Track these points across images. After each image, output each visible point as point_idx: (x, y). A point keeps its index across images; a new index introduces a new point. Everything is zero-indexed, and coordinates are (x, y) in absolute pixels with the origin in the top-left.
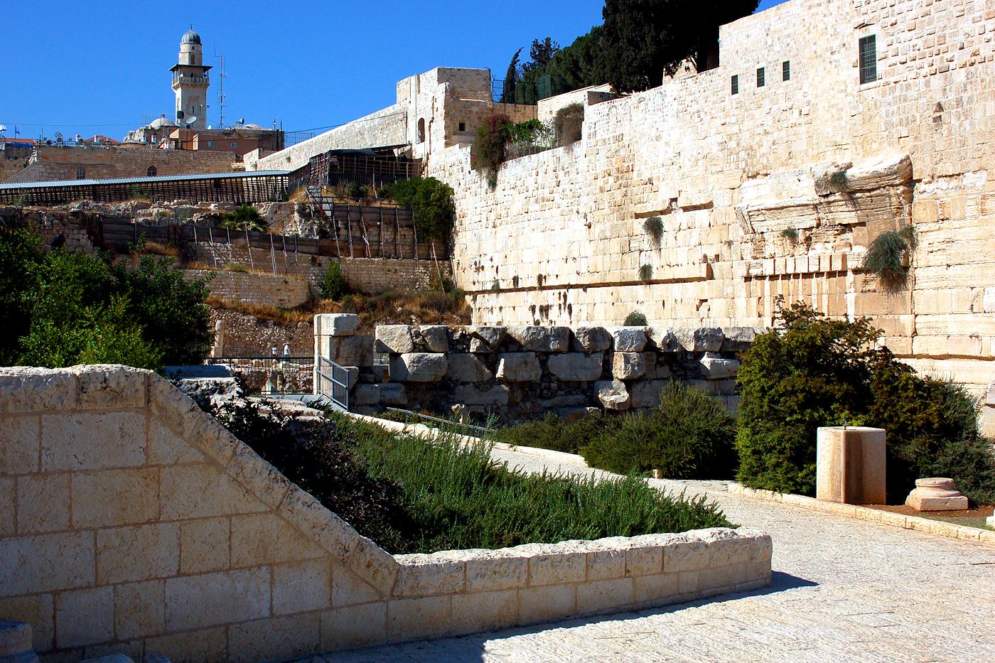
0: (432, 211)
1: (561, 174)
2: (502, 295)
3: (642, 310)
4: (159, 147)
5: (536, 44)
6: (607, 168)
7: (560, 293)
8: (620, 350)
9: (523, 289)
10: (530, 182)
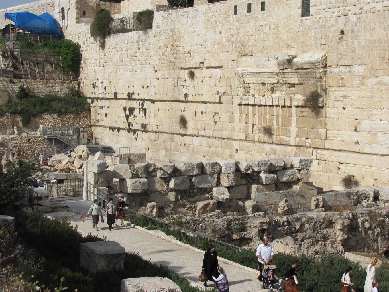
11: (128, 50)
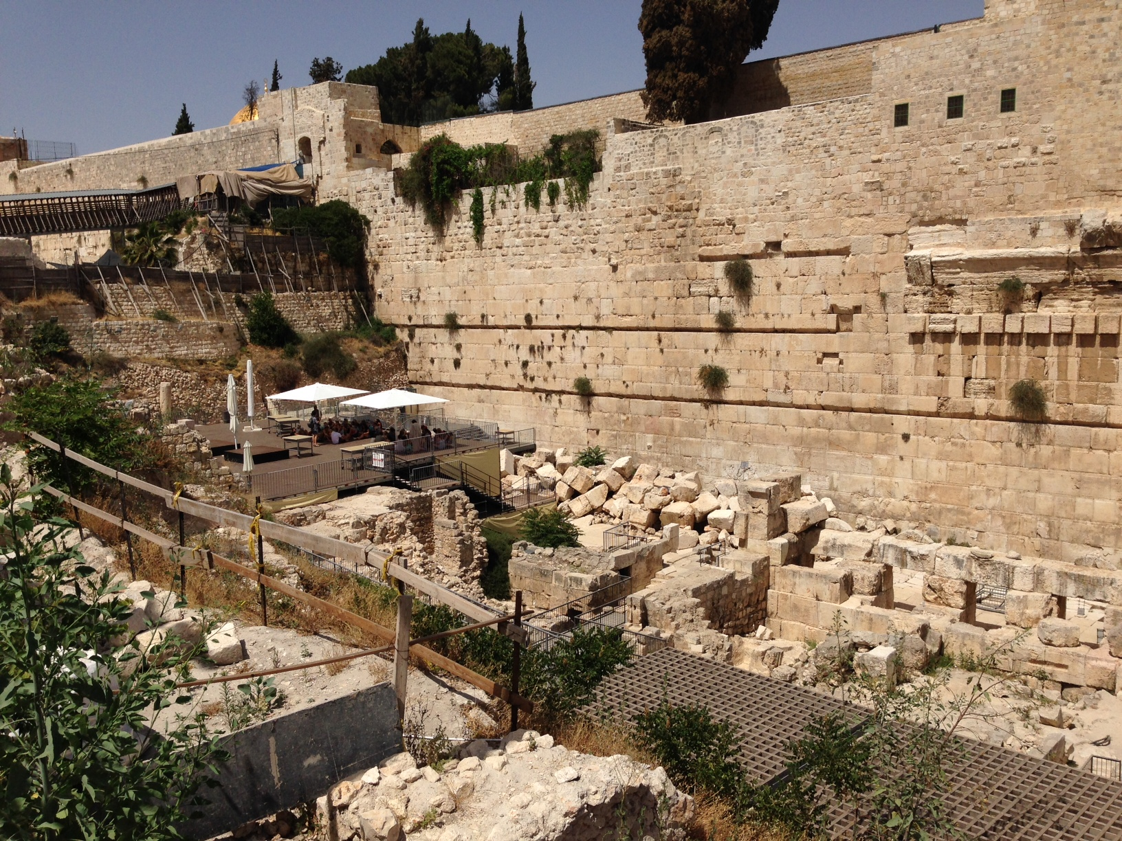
5: (316, 63)
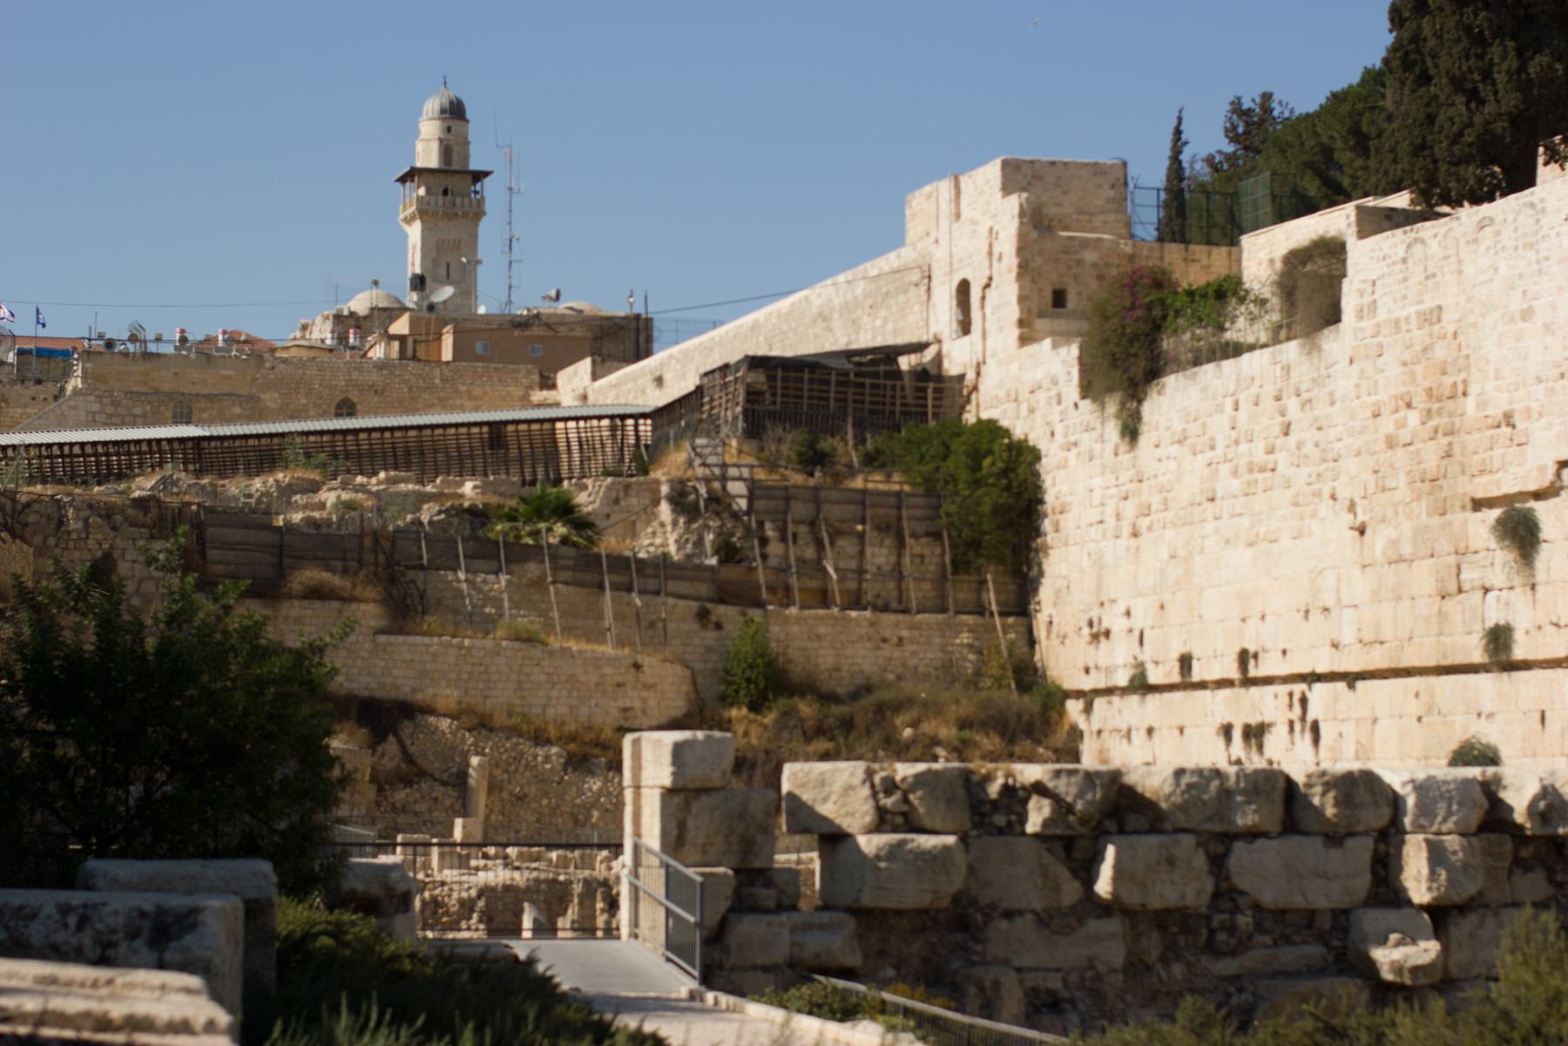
0: (988, 500)
1: (1292, 404)
2: (1154, 700)
3: (1489, 734)
4: (364, 356)
5: (1237, 108)
6: (1403, 389)
7: (1291, 695)
8: (1419, 828)
9: (1202, 685)
10: (1219, 427)
11: (1237, 442)
